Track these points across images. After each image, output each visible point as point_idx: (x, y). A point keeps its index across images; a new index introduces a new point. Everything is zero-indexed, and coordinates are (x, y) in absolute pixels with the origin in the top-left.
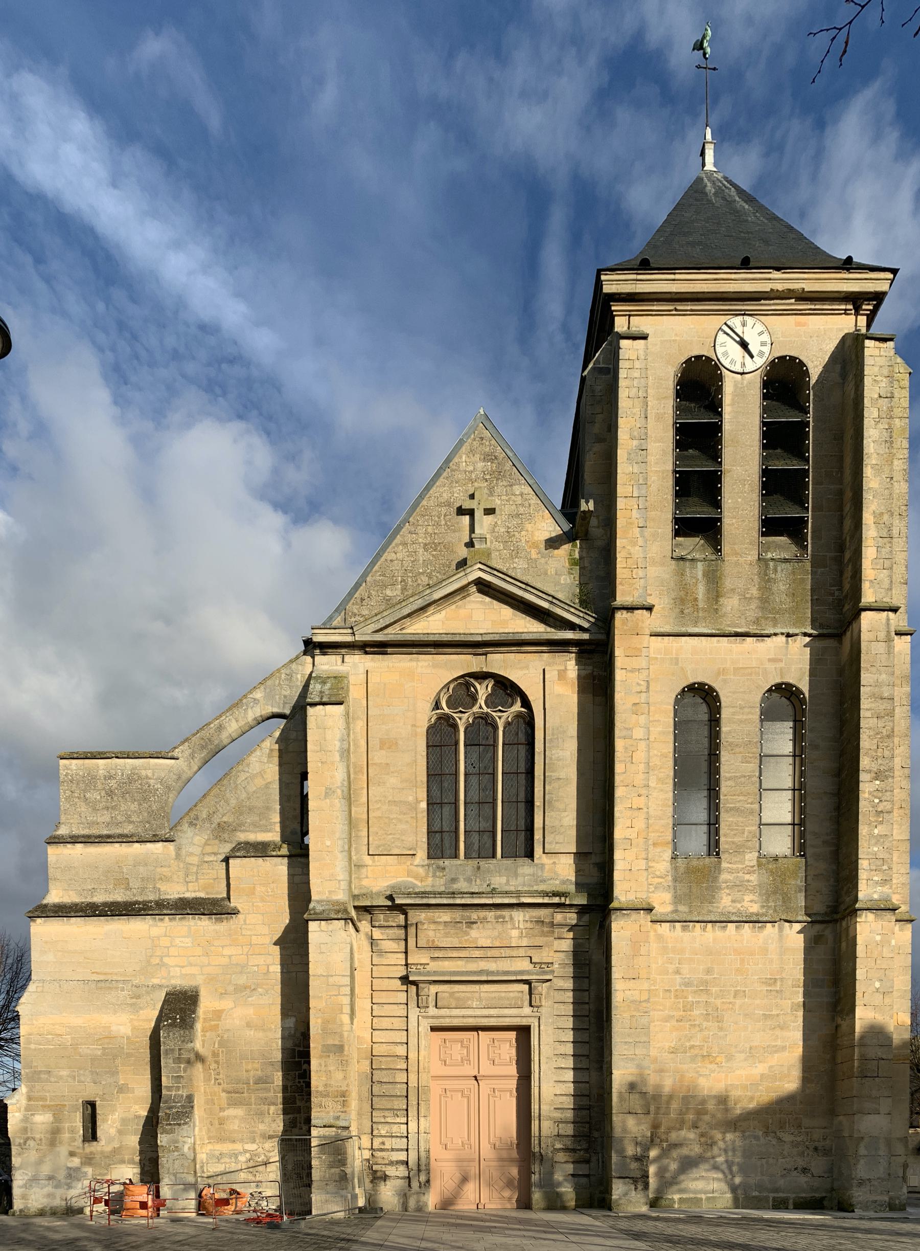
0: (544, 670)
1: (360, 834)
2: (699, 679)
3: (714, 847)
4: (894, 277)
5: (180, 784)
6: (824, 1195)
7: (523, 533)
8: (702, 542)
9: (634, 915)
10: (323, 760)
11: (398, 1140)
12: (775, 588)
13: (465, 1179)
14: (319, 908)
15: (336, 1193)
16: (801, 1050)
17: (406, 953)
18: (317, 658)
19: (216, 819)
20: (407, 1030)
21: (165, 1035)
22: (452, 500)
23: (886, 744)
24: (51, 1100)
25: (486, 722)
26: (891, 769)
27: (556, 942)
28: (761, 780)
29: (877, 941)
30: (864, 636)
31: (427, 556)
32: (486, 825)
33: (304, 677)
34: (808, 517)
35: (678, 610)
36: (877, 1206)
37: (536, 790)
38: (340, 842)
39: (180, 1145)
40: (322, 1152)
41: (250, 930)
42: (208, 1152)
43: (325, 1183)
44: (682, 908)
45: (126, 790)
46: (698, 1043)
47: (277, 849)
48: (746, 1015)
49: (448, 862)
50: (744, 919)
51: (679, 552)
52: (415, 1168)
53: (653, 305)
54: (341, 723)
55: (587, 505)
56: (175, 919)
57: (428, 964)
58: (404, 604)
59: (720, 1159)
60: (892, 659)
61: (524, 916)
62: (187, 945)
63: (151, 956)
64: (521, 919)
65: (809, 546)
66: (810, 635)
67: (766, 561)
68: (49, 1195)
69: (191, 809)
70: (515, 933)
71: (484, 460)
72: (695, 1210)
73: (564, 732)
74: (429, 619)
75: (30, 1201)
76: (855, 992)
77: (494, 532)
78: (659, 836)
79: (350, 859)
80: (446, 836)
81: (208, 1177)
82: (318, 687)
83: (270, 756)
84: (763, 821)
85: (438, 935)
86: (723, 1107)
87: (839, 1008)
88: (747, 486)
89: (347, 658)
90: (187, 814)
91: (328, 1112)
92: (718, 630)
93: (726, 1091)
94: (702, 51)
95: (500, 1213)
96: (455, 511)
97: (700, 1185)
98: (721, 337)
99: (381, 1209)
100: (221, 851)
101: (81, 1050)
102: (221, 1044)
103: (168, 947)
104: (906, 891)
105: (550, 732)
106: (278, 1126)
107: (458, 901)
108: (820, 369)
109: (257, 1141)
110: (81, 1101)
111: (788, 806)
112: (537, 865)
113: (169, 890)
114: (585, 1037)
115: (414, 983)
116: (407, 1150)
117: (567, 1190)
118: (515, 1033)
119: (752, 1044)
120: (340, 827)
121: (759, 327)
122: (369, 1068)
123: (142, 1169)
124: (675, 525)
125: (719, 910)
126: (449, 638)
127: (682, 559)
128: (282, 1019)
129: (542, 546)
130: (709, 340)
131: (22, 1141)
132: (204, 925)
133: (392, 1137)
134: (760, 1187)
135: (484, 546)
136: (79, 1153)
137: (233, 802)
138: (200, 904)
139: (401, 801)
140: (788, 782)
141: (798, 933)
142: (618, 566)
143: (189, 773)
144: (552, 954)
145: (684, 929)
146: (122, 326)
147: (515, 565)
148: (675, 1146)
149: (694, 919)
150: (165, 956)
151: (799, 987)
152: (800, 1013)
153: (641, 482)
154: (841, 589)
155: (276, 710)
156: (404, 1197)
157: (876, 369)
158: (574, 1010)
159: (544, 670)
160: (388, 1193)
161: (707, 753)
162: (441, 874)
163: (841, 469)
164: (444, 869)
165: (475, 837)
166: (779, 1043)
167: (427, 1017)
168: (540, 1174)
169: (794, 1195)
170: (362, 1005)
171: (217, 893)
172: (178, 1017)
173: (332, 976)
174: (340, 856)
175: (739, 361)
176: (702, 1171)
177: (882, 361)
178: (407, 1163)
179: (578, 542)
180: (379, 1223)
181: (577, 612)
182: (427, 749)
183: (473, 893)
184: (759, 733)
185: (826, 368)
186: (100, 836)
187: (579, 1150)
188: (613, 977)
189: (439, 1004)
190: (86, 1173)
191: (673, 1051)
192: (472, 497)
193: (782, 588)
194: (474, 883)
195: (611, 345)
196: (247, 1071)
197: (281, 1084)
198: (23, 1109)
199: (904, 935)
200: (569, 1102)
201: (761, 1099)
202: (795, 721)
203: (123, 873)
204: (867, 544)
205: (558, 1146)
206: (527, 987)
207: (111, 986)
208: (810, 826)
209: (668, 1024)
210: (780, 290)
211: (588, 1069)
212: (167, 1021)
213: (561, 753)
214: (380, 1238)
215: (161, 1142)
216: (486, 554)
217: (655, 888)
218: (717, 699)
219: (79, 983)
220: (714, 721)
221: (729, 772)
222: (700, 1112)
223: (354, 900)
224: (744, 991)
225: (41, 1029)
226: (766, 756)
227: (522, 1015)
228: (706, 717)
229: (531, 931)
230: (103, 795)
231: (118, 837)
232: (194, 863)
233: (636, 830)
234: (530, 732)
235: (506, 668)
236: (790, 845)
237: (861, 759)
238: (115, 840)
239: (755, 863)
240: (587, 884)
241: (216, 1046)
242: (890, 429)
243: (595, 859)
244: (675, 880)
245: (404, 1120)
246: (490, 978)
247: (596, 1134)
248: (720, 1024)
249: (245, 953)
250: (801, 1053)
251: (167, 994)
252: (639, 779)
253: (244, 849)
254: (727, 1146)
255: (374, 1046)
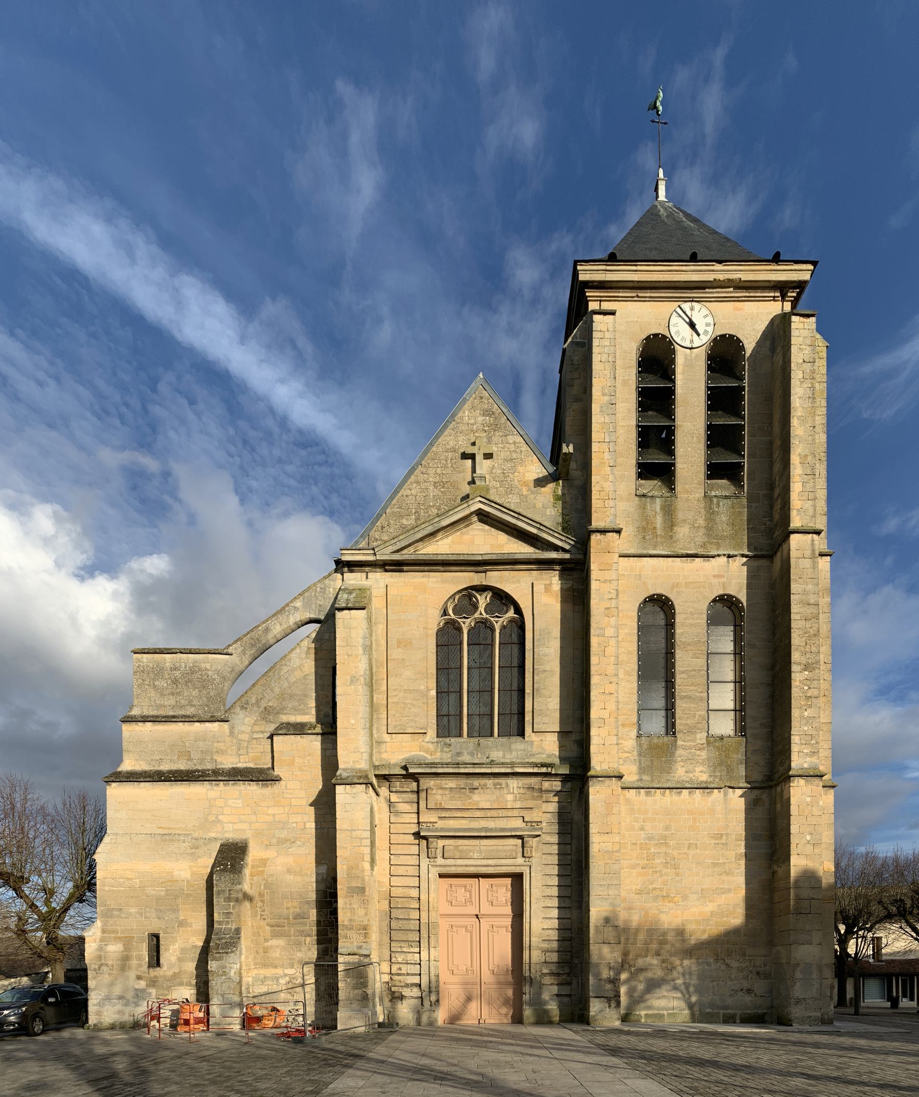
0: (532, 584)
1: (380, 716)
2: (658, 591)
3: (671, 728)
4: (814, 268)
5: (234, 675)
6: (765, 1011)
7: (516, 474)
8: (659, 483)
9: (607, 781)
10: (349, 654)
11: (413, 966)
12: (718, 519)
13: (469, 999)
14: (345, 775)
15: (359, 1011)
16: (744, 891)
17: (418, 813)
18: (345, 575)
19: (263, 704)
20: (419, 877)
21: (217, 879)
22: (457, 447)
23: (812, 642)
24: (122, 933)
25: (486, 626)
26: (818, 662)
27: (544, 805)
28: (708, 673)
29: (807, 802)
30: (793, 554)
31: (437, 492)
32: (485, 710)
33: (335, 590)
34: (744, 462)
35: (641, 537)
36: (811, 1021)
37: (527, 680)
38: (363, 721)
39: (227, 970)
40: (347, 976)
41: (291, 794)
42: (254, 975)
43: (349, 1002)
44: (645, 777)
45: (188, 679)
46: (659, 886)
47: (312, 729)
48: (698, 863)
49: (453, 740)
50: (696, 786)
51: (642, 491)
52: (427, 990)
53: (620, 292)
54: (364, 624)
55: (567, 449)
56: (229, 784)
57: (436, 822)
58: (417, 529)
59: (679, 982)
60: (816, 572)
61: (518, 783)
62: (238, 806)
63: (208, 815)
64: (515, 786)
65: (745, 486)
66: (746, 556)
67: (711, 498)
68: (119, 1012)
69: (242, 696)
70: (510, 797)
71: (483, 415)
72: (659, 1024)
73: (549, 633)
74: (440, 543)
75: (103, 1017)
76: (790, 843)
77: (492, 473)
78: (627, 719)
79: (371, 735)
80: (452, 719)
81: (254, 997)
82: (345, 596)
83: (307, 653)
84: (711, 708)
85: (444, 798)
86: (680, 938)
87: (775, 858)
88: (695, 438)
89: (370, 575)
90: (239, 699)
91: (352, 943)
92: (673, 552)
93: (683, 925)
94: (655, 110)
95: (497, 1027)
96: (460, 456)
97: (662, 1003)
98: (675, 319)
99: (397, 1024)
100: (267, 729)
101: (147, 892)
102: (266, 887)
103: (222, 807)
104: (829, 762)
105: (538, 633)
106: (313, 954)
107: (462, 771)
108: (754, 345)
109: (296, 966)
110: (147, 934)
111: (731, 696)
112: (527, 742)
113: (224, 761)
114: (568, 881)
115: (425, 838)
116: (420, 975)
117: (553, 1007)
118: (510, 879)
119: (704, 887)
120: (363, 709)
121: (705, 311)
122: (387, 907)
123: (198, 990)
124: (638, 468)
125: (675, 779)
126: (455, 557)
127: (644, 496)
128: (316, 867)
129: (532, 485)
130: (664, 321)
131: (97, 967)
132: (253, 789)
133: (408, 963)
134: (712, 1005)
135: (483, 483)
136: (145, 977)
137: (277, 690)
138: (249, 773)
139: (415, 690)
140: (730, 676)
141: (740, 797)
142: (593, 497)
143: (242, 667)
144: (540, 814)
145: (647, 794)
146: (245, 442)
147: (509, 500)
148: (641, 970)
149: (656, 786)
150: (220, 814)
151: (741, 840)
152: (743, 862)
153: (611, 430)
154: (771, 520)
155: (313, 616)
156: (418, 1013)
157: (801, 339)
158: (559, 860)
159: (532, 584)
160: (405, 1011)
161: (664, 652)
162: (448, 750)
163: (771, 424)
164: (450, 745)
165: (476, 720)
166: (726, 886)
167: (436, 866)
168: (530, 994)
169: (740, 1012)
170: (382, 855)
171: (264, 764)
172: (229, 863)
173: (355, 830)
174: (362, 732)
175: (688, 338)
176: (664, 991)
177: (806, 333)
178: (420, 986)
179: (561, 482)
180: (393, 1037)
181: (560, 537)
182: (437, 648)
183: (474, 764)
184: (706, 635)
185: (759, 344)
186: (166, 717)
187: (563, 974)
188: (591, 832)
189: (446, 855)
190: (150, 994)
191: (639, 893)
192: (474, 444)
193: (724, 519)
194: (475, 756)
195: (586, 324)
196: (287, 908)
197: (315, 919)
198: (98, 940)
199: (829, 798)
200: (554, 935)
201: (712, 932)
202: (735, 626)
203: (186, 746)
204: (794, 480)
205: (545, 971)
206: (520, 841)
207: (174, 838)
208: (750, 711)
209: (635, 871)
210: (722, 280)
211: (570, 908)
212: (220, 867)
213: (546, 650)
214: (386, 1053)
215: (211, 967)
216: (485, 490)
217: (624, 761)
218: (672, 607)
219: (147, 836)
220: (670, 625)
221: (682, 667)
222: (663, 943)
223: (374, 769)
224: (696, 844)
225: (114, 874)
226: (711, 654)
227: (516, 864)
228: (663, 622)
229: (523, 796)
230: (169, 683)
231: (182, 718)
232: (245, 739)
233: (608, 711)
234: (521, 634)
235: (501, 582)
236: (732, 727)
237: (792, 653)
238: (178, 720)
239: (704, 741)
240: (569, 758)
241: (262, 888)
242: (813, 388)
243: (574, 737)
244: (640, 755)
245: (417, 950)
246: (488, 834)
247: (576, 961)
248: (677, 871)
249: (286, 812)
250: (744, 895)
251: (221, 845)
252: (611, 669)
253: (285, 728)
254: (684, 971)
255: (392, 889)
